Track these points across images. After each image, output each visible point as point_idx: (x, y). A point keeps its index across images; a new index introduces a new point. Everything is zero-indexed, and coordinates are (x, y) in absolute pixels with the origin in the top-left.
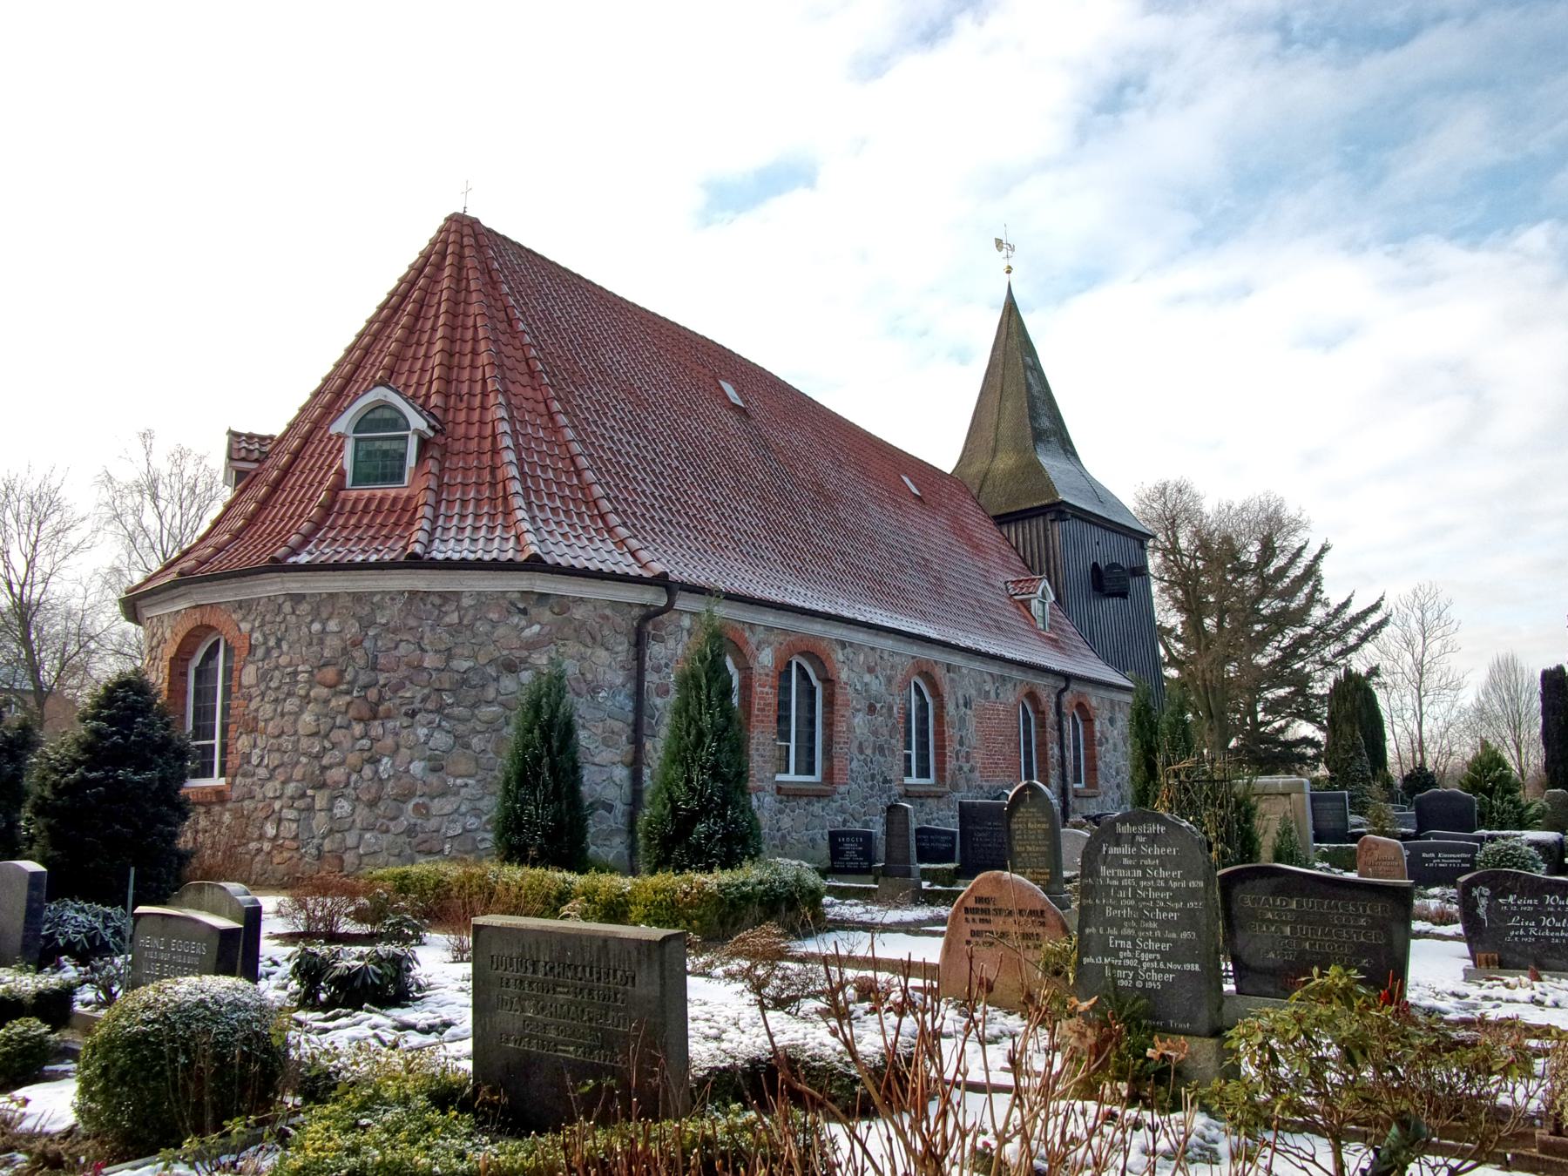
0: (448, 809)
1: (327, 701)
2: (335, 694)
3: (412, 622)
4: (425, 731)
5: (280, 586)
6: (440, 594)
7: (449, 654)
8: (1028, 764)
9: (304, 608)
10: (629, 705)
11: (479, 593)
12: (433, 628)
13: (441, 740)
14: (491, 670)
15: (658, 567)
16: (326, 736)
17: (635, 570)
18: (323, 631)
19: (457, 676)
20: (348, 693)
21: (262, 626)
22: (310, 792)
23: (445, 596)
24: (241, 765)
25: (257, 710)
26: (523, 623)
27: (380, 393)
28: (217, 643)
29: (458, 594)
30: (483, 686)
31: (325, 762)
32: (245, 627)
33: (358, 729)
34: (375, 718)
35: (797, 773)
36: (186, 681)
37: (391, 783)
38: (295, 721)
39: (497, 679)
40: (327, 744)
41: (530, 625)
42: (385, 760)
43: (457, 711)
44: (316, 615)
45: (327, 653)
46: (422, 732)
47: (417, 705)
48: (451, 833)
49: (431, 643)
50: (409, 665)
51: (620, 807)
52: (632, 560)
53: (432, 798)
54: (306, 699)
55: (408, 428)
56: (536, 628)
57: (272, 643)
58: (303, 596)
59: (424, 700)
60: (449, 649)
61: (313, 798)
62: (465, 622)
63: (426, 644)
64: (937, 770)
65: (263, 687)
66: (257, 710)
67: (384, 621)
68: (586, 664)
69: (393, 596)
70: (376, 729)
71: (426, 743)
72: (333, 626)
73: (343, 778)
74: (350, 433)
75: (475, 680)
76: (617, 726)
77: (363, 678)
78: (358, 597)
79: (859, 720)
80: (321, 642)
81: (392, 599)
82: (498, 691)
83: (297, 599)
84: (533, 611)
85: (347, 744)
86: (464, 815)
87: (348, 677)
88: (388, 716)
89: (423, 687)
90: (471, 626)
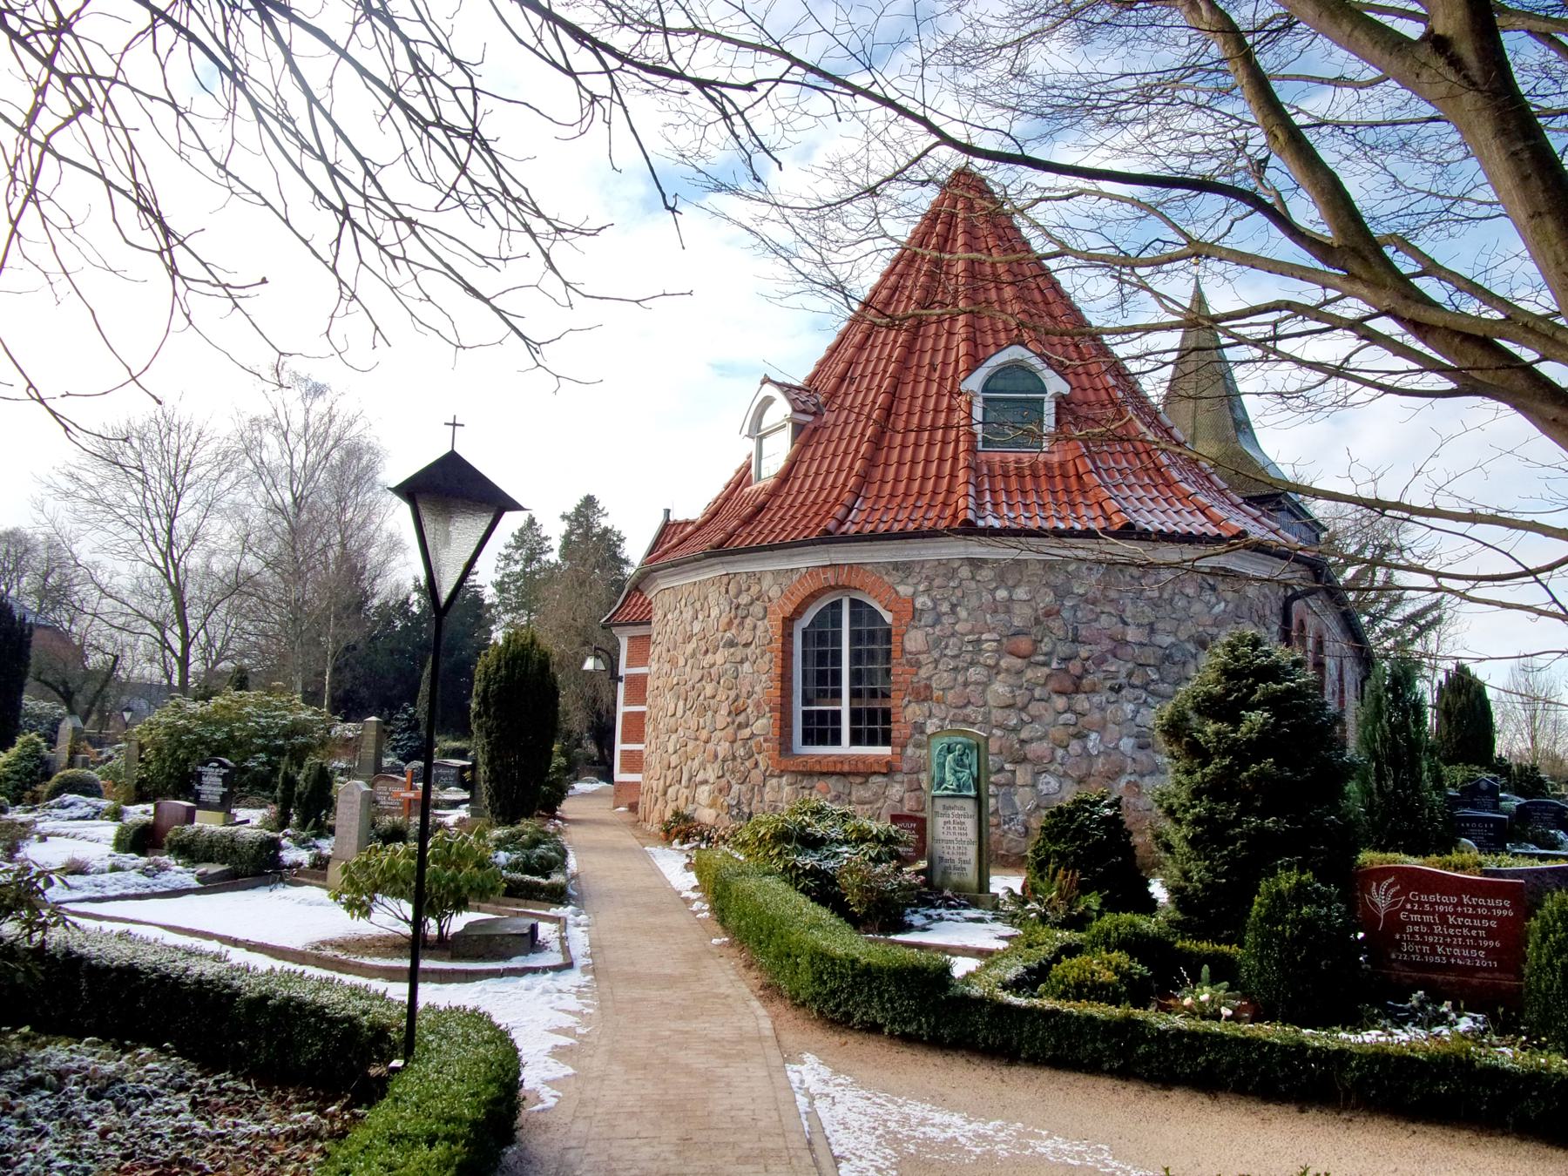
1: (1020, 673)
2: (1030, 664)
3: (1113, 594)
5: (962, 549)
7: (1152, 629)
9: (986, 574)
12: (1134, 602)
14: (1191, 647)
16: (1024, 708)
17: (1212, 530)
18: (1010, 599)
19: (1161, 652)
20: (1045, 664)
21: (927, 591)
22: (1008, 766)
24: (912, 735)
25: (930, 678)
26: (1213, 600)
27: (1014, 353)
28: (837, 605)
30: (1184, 663)
31: (1024, 735)
32: (902, 589)
33: (1060, 702)
34: (1077, 690)
35: (856, 739)
37: (1101, 760)
38: (984, 691)
39: (1194, 657)
40: (1026, 718)
42: (1094, 736)
44: (1001, 579)
45: (1017, 622)
46: (1129, 707)
47: (1123, 681)
49: (1134, 616)
50: (1111, 638)
52: (1204, 520)
53: (1142, 776)
54: (995, 669)
57: (945, 608)
58: (985, 561)
59: (1130, 675)
60: (1151, 624)
62: (1166, 596)
63: (1128, 616)
66: (930, 678)
67: (1081, 591)
70: (1081, 702)
71: (1133, 719)
72: (1021, 593)
73: (1048, 752)
75: (1178, 657)
77: (1063, 649)
80: (1008, 611)
81: (1090, 569)
83: (976, 564)
84: (1221, 587)
85: (1049, 717)
87: (1045, 647)
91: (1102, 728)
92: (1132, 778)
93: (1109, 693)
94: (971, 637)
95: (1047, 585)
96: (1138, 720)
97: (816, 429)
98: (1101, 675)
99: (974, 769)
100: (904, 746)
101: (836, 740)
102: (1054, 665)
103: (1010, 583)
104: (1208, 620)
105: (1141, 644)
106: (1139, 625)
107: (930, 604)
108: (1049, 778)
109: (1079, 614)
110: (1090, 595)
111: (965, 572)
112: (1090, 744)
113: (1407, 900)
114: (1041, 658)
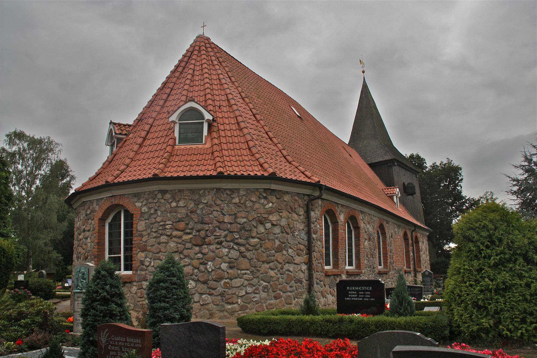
4: (227, 250)
6: (230, 190)
7: (236, 216)
8: (350, 257)
9: (168, 196)
10: (306, 238)
11: (247, 189)
13: (234, 254)
14: (254, 223)
15: (315, 179)
17: (303, 178)
18: (177, 207)
19: (239, 226)
23: (232, 191)
26: (266, 202)
36: (105, 229)
37: (213, 273)
40: (182, 257)
41: (268, 203)
42: (210, 263)
43: (240, 241)
44: (174, 198)
45: (179, 216)
48: (240, 294)
53: (231, 280)
55: (203, 118)
56: (271, 205)
60: (235, 214)
64: (384, 263)
65: (149, 231)
67: (205, 202)
68: (290, 220)
72: (181, 204)
74: (177, 121)
76: (302, 247)
79: (366, 243)
81: (209, 192)
82: (257, 233)
83: (164, 192)
84: (269, 197)
86: (245, 286)
88: (210, 244)
89: (225, 231)
90: (244, 204)
91: (213, 260)
92: (227, 281)
93: (216, 245)
94: (161, 223)
96: (229, 256)
97: (126, 140)
98: (213, 237)
99: (87, 280)
100: (137, 271)
101: (120, 270)
102: (194, 234)
103: (177, 199)
105: (231, 223)
107: (147, 210)
109: (204, 212)
110: (209, 203)
111: (159, 196)
112: (208, 267)
114: (189, 231)
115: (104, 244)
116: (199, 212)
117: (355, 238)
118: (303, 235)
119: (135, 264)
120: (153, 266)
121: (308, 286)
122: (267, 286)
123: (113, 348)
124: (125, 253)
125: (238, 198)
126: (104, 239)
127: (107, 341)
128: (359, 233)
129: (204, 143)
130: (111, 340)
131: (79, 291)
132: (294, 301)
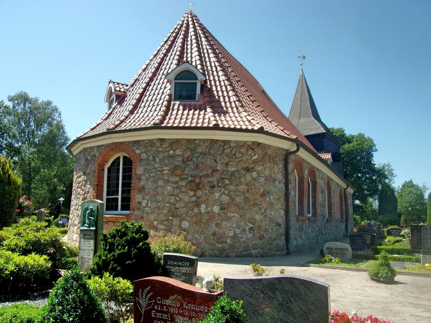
0: (228, 225)
9: (166, 145)
28: (119, 158)
29: (229, 141)
33: (192, 193)
35: (122, 209)
41: (255, 155)
48: (230, 235)
51: (283, 226)
55: (197, 79)
56: (257, 156)
57: (151, 158)
61: (172, 220)
69: (204, 141)
70: (199, 193)
71: (219, 199)
72: (178, 152)
74: (173, 80)
78: (189, 141)
81: (204, 142)
83: (162, 140)
84: (256, 150)
95: (188, 148)
99: (95, 217)
101: (117, 209)
104: (251, 162)
106: (222, 164)
108: (186, 222)
111: (158, 144)
113: (155, 303)
114: (184, 176)
115: (103, 186)
116: (194, 159)
117: (312, 190)
118: (282, 186)
119: (133, 204)
120: (150, 207)
121: (285, 229)
122: (253, 227)
123: (159, 315)
124: (122, 195)
125: (229, 149)
126: (103, 182)
127: (149, 304)
128: (316, 186)
129: (197, 100)
130: (155, 303)
131: (86, 228)
132: (274, 242)
